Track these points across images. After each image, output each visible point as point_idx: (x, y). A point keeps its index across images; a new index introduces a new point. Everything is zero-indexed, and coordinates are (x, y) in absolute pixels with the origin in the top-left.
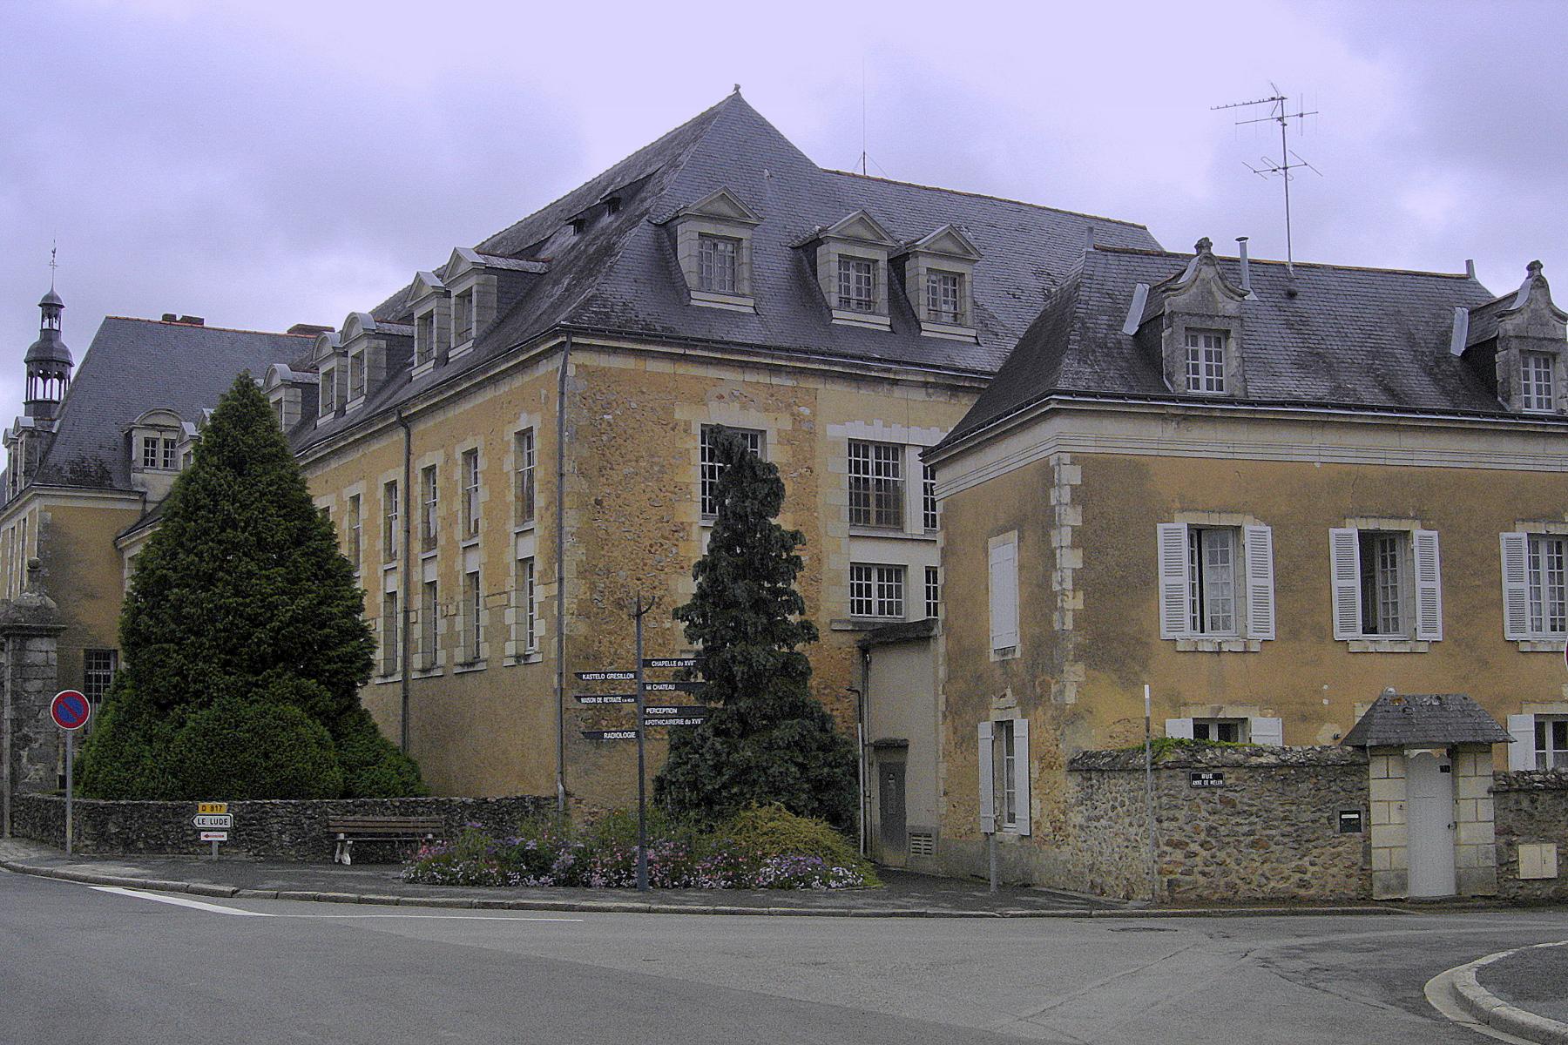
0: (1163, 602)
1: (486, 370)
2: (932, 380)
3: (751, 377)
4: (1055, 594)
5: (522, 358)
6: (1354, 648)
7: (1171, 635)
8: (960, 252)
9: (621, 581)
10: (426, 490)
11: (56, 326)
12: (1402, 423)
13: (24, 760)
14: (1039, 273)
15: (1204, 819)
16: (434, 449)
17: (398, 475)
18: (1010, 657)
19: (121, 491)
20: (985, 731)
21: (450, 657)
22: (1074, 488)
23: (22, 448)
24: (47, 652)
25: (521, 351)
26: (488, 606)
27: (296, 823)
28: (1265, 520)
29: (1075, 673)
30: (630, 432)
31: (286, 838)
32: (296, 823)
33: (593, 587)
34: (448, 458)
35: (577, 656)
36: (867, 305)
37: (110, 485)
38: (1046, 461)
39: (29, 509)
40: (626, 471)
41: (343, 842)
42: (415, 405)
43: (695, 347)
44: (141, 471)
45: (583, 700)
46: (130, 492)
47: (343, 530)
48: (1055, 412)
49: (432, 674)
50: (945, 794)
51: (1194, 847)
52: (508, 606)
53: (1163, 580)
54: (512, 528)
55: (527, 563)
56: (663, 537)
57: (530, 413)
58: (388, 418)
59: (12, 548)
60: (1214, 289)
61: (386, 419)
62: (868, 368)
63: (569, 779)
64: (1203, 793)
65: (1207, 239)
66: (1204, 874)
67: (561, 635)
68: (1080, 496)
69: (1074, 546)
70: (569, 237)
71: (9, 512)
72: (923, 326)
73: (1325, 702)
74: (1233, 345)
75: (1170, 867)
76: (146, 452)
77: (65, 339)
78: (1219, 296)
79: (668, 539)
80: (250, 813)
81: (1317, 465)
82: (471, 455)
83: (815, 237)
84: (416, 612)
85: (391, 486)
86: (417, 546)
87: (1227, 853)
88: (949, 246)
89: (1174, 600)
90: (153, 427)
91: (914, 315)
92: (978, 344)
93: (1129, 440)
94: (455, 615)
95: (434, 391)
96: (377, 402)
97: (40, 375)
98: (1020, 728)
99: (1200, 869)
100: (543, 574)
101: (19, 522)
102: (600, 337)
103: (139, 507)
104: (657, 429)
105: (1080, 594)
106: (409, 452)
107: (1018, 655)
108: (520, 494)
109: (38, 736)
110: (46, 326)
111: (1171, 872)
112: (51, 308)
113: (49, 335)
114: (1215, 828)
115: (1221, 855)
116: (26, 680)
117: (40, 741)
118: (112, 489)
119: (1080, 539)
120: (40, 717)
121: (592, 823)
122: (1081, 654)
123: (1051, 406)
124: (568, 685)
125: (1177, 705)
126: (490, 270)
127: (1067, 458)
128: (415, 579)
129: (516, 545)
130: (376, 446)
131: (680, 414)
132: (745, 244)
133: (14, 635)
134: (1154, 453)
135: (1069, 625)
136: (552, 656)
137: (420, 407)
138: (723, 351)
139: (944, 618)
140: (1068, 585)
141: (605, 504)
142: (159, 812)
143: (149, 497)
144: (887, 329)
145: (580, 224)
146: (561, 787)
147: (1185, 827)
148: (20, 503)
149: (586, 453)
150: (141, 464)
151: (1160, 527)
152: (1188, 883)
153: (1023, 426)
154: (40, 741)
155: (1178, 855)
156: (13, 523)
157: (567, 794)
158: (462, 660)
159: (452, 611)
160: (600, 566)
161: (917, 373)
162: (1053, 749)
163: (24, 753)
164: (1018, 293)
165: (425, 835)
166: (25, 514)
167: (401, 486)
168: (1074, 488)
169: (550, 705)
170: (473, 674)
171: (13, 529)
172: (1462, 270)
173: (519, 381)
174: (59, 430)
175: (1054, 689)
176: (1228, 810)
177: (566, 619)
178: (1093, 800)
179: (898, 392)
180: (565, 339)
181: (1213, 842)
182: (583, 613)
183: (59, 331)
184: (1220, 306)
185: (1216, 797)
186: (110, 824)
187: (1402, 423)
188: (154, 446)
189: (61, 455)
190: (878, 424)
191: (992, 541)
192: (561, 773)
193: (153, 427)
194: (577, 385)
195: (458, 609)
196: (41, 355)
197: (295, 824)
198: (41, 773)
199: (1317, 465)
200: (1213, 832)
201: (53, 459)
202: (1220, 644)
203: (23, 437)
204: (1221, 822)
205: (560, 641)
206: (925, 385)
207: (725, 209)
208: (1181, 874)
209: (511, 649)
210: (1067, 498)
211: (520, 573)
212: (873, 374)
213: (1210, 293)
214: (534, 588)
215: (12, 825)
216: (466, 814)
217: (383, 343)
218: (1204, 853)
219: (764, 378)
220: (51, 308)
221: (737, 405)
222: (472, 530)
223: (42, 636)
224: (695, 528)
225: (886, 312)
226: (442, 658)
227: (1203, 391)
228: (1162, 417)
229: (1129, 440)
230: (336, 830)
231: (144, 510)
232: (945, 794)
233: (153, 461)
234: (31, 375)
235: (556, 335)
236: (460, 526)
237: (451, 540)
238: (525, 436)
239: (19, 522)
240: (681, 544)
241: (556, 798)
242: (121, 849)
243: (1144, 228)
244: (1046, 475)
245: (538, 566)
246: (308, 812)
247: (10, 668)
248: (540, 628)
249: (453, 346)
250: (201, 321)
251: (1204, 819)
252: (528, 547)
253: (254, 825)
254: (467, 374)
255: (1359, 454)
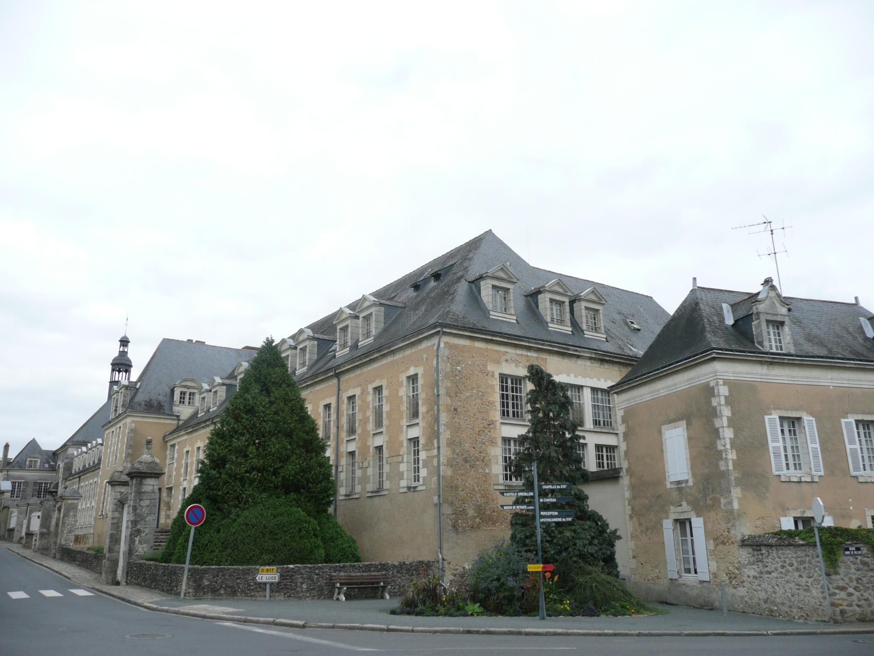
0: (772, 455)
1: (390, 347)
2: (594, 356)
3: (519, 352)
4: (721, 452)
5: (413, 340)
6: (861, 480)
7: (777, 473)
8: (597, 299)
9: (466, 449)
10: (348, 408)
11: (126, 350)
12: (867, 367)
13: (137, 542)
14: (619, 313)
15: (854, 574)
16: (354, 387)
17: (332, 401)
18: (684, 485)
19: (168, 415)
20: (668, 524)
21: (364, 489)
22: (726, 397)
23: (121, 396)
24: (153, 485)
25: (413, 337)
26: (389, 462)
27: (310, 578)
28: (811, 414)
29: (736, 493)
30: (468, 375)
31: (304, 586)
32: (310, 578)
33: (454, 452)
34: (364, 392)
35: (447, 487)
36: (561, 322)
37: (164, 412)
38: (707, 384)
39: (123, 422)
40: (467, 394)
41: (339, 588)
42: (344, 367)
43: (496, 336)
44: (178, 406)
45: (505, 508)
46: (173, 415)
47: (320, 423)
48: (714, 359)
49: (352, 497)
50: (634, 557)
51: (851, 590)
52: (402, 462)
53: (771, 445)
54: (404, 423)
55: (415, 441)
56: (484, 427)
57: (416, 366)
58: (328, 373)
59: (112, 440)
60: (775, 301)
61: (326, 374)
62: (568, 349)
63: (445, 551)
64: (851, 559)
65: (770, 278)
66: (859, 606)
67: (439, 475)
68: (729, 401)
69: (729, 426)
70: (411, 293)
71: (111, 424)
72: (585, 332)
73: (851, 508)
74: (786, 329)
75: (840, 602)
76: (181, 398)
77: (129, 356)
78: (778, 305)
79: (486, 428)
80: (287, 572)
81: (831, 387)
82: (378, 389)
83: (538, 290)
84: (343, 466)
85: (328, 407)
86: (344, 435)
87: (869, 593)
88: (593, 297)
89: (777, 455)
90: (185, 386)
91: (580, 328)
92: (607, 341)
93: (748, 373)
94: (367, 467)
95: (358, 359)
96: (316, 368)
97: (117, 371)
98: (698, 523)
99: (856, 603)
100: (424, 446)
101: (116, 429)
102: (455, 329)
103: (175, 422)
104: (480, 374)
105: (734, 451)
106: (339, 390)
107: (691, 483)
108: (408, 406)
109: (145, 529)
110: (121, 350)
111: (841, 605)
112: (124, 342)
113: (123, 354)
114: (860, 579)
115: (866, 595)
116: (141, 500)
117: (146, 533)
118: (164, 414)
119: (731, 422)
120: (147, 519)
121: (456, 575)
122: (739, 482)
123: (712, 356)
124: (443, 502)
125: (785, 511)
126: (381, 304)
127: (721, 382)
128: (341, 450)
129: (407, 431)
130: (318, 387)
131: (490, 367)
132: (511, 291)
133: (136, 476)
134: (759, 380)
135: (731, 467)
136: (433, 487)
137: (347, 367)
138: (508, 338)
139: (627, 467)
140: (728, 446)
141: (458, 410)
142: (234, 572)
143: (181, 418)
144: (570, 333)
145: (416, 287)
146: (440, 556)
147: (845, 578)
148: (118, 419)
149: (449, 384)
150: (178, 403)
151: (766, 417)
152: (851, 611)
153: (687, 369)
154: (146, 533)
155: (843, 595)
156: (113, 429)
157: (443, 559)
158: (372, 490)
159: (366, 464)
160: (457, 441)
161: (588, 353)
162: (726, 534)
163: (137, 539)
164: (614, 321)
165: (379, 583)
166: (121, 424)
167: (333, 406)
168: (726, 397)
169: (431, 513)
170: (379, 497)
171: (113, 432)
172: (853, 302)
173: (408, 352)
174: (140, 387)
175: (723, 501)
176: (866, 568)
177: (442, 468)
178: (763, 562)
179: (580, 362)
180: (440, 329)
181: (861, 587)
182: (450, 464)
183: (127, 352)
184: (779, 309)
185: (858, 561)
186: (205, 579)
187: (867, 367)
188: (184, 394)
189: (141, 397)
190: (572, 375)
191: (664, 428)
192: (440, 548)
193: (185, 386)
194: (444, 352)
195: (369, 464)
196: (118, 362)
197: (309, 578)
198: (145, 549)
199: (831, 387)
200: (860, 581)
201: (137, 399)
202: (800, 478)
203: (123, 390)
204: (863, 575)
205: (439, 478)
206: (591, 358)
207: (501, 274)
208: (846, 606)
209: (404, 483)
210: (723, 402)
211: (409, 445)
212: (570, 352)
213: (774, 303)
214: (420, 453)
215: (127, 578)
216: (395, 571)
217: (316, 343)
218: (857, 594)
219: (524, 352)
220: (124, 342)
221: (514, 365)
222: (379, 423)
223: (151, 477)
224: (498, 424)
225: (569, 325)
226: (358, 489)
227: (774, 350)
228: (761, 363)
229: (748, 373)
230: (335, 581)
231: (178, 423)
232: (634, 557)
233: (183, 402)
234: (113, 370)
235: (435, 327)
236: (371, 424)
237: (365, 430)
238: (413, 379)
239: (116, 429)
240: (492, 431)
241: (438, 562)
242: (210, 594)
243: (651, 297)
244: (709, 391)
245: (422, 441)
246: (317, 571)
247: (133, 494)
248: (423, 473)
249: (360, 340)
250: (204, 343)
251: (854, 574)
252: (414, 433)
253: (288, 579)
254: (366, 355)
255: (850, 382)
